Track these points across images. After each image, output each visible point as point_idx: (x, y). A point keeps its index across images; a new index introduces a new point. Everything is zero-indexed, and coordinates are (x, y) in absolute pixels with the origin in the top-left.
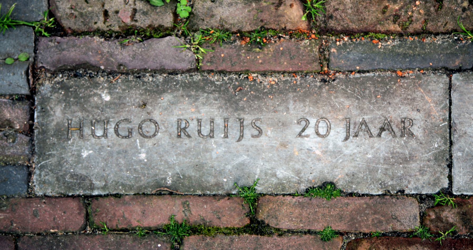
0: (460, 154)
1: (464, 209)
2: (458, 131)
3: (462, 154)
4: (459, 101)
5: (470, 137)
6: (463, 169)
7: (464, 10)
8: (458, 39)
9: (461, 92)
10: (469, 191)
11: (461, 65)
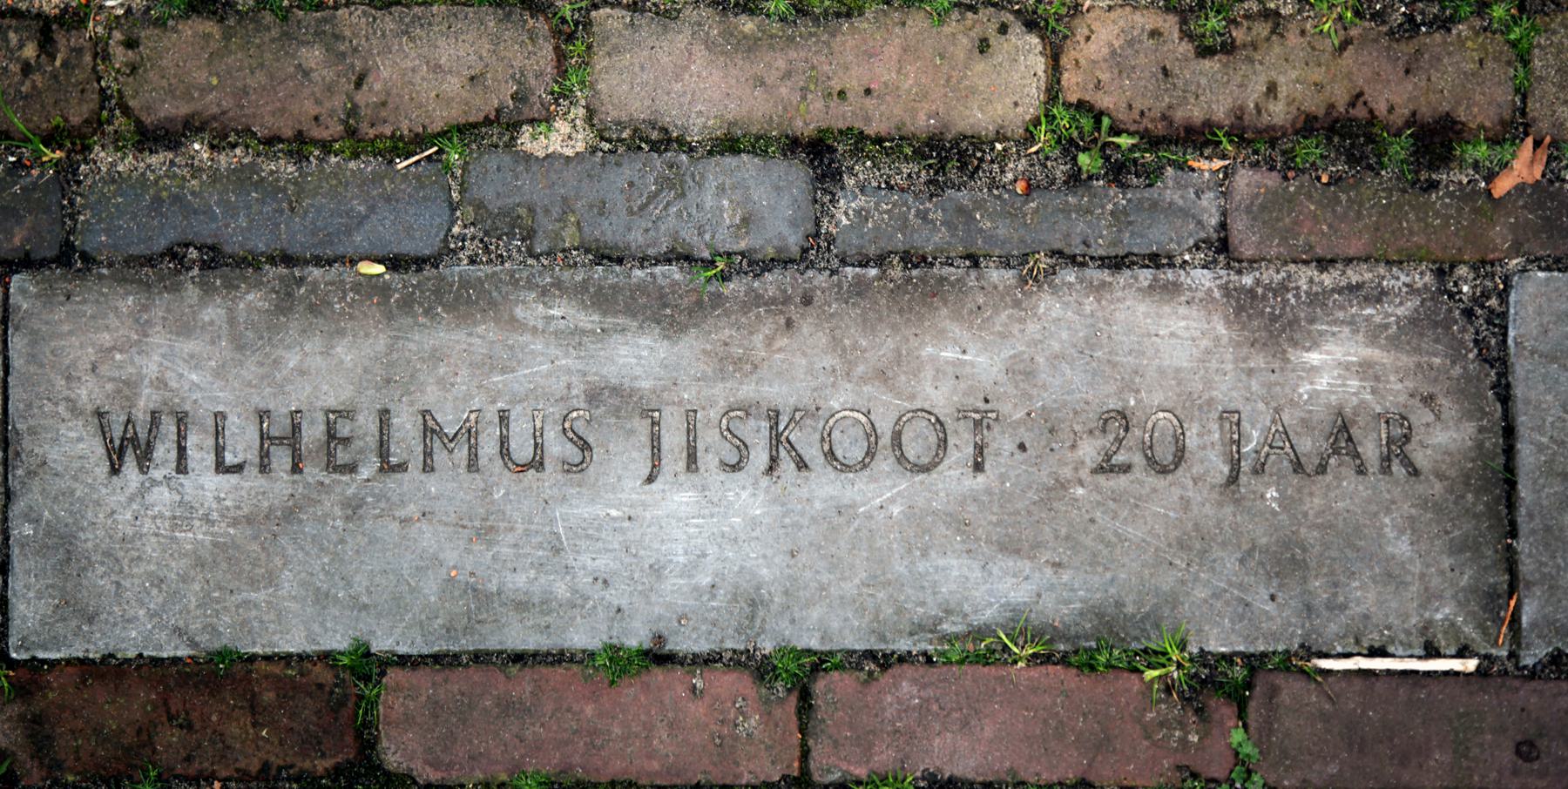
0: (28, 530)
1: (38, 705)
2: (23, 456)
3: (35, 529)
4: (28, 362)
5: (57, 475)
6: (36, 576)
7: (27, 69)
8: (19, 164)
9: (34, 332)
10: (50, 646)
11: (28, 247)
